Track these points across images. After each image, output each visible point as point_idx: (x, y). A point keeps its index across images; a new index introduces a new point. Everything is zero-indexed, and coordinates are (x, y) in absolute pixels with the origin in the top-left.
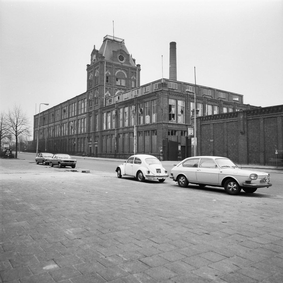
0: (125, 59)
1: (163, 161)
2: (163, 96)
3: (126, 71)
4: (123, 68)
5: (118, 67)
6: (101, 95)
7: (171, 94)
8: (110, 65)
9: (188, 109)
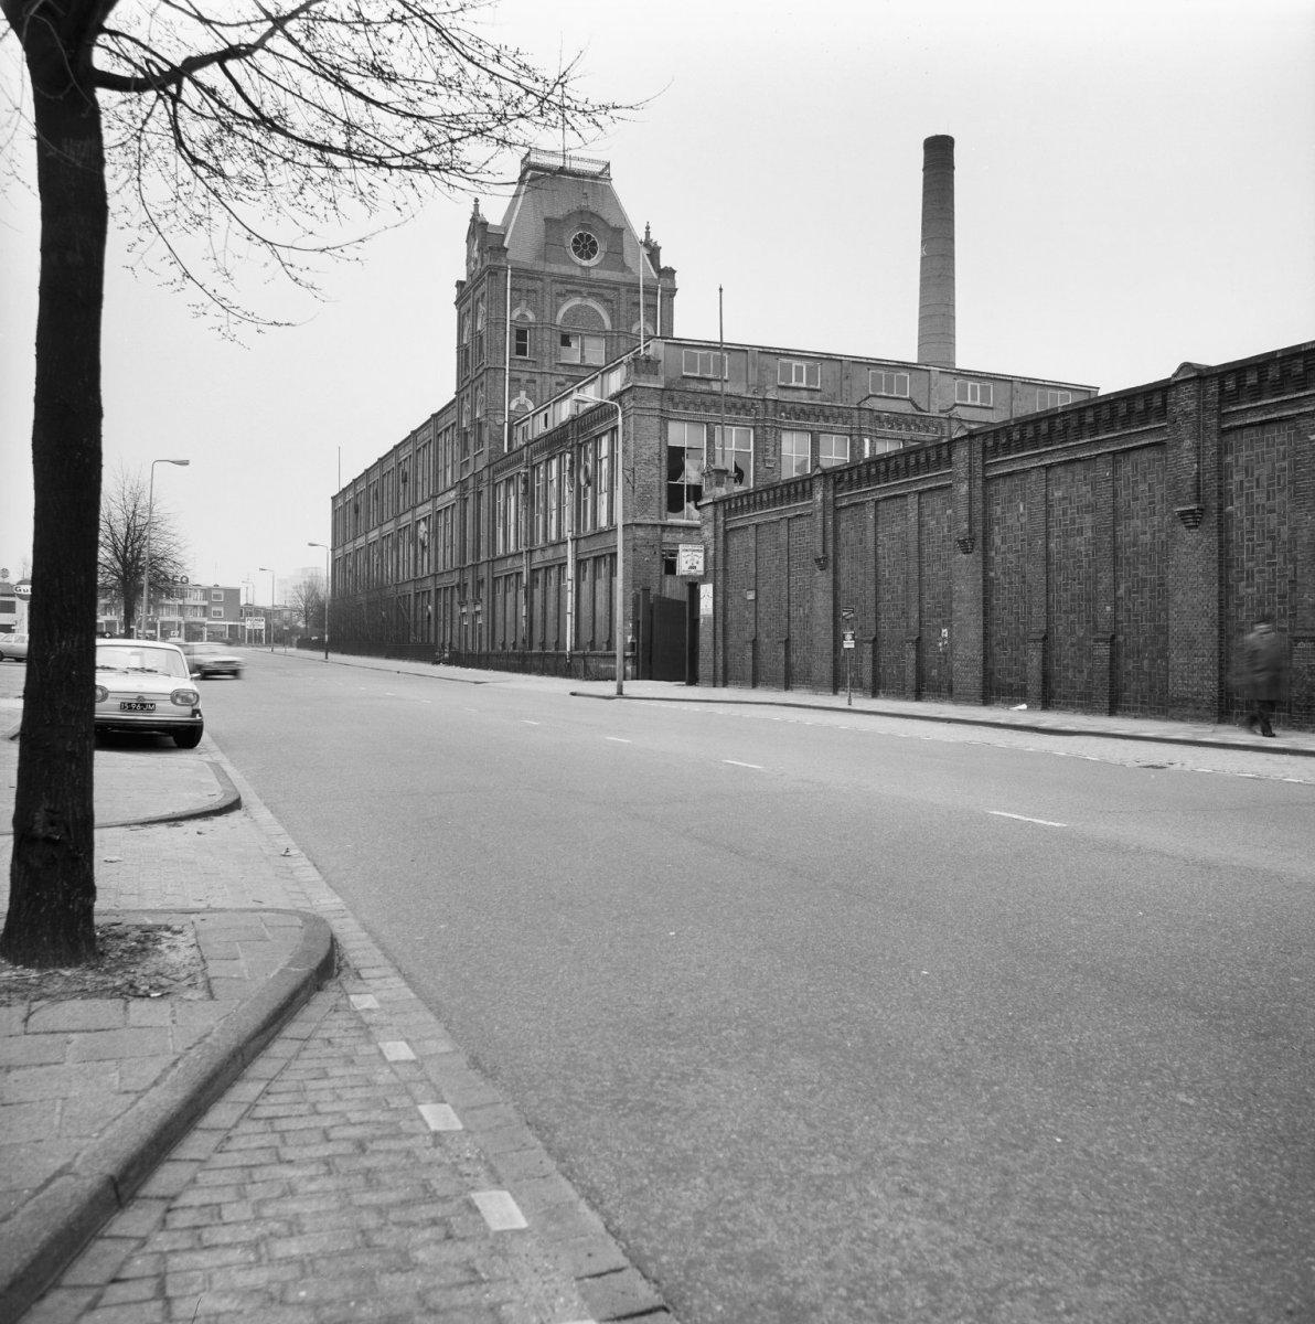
0: (601, 247)
1: (632, 679)
2: (639, 412)
3: (608, 301)
4: (594, 288)
5: (569, 287)
6: (495, 408)
7: (677, 400)
8: (532, 279)
9: (764, 461)
